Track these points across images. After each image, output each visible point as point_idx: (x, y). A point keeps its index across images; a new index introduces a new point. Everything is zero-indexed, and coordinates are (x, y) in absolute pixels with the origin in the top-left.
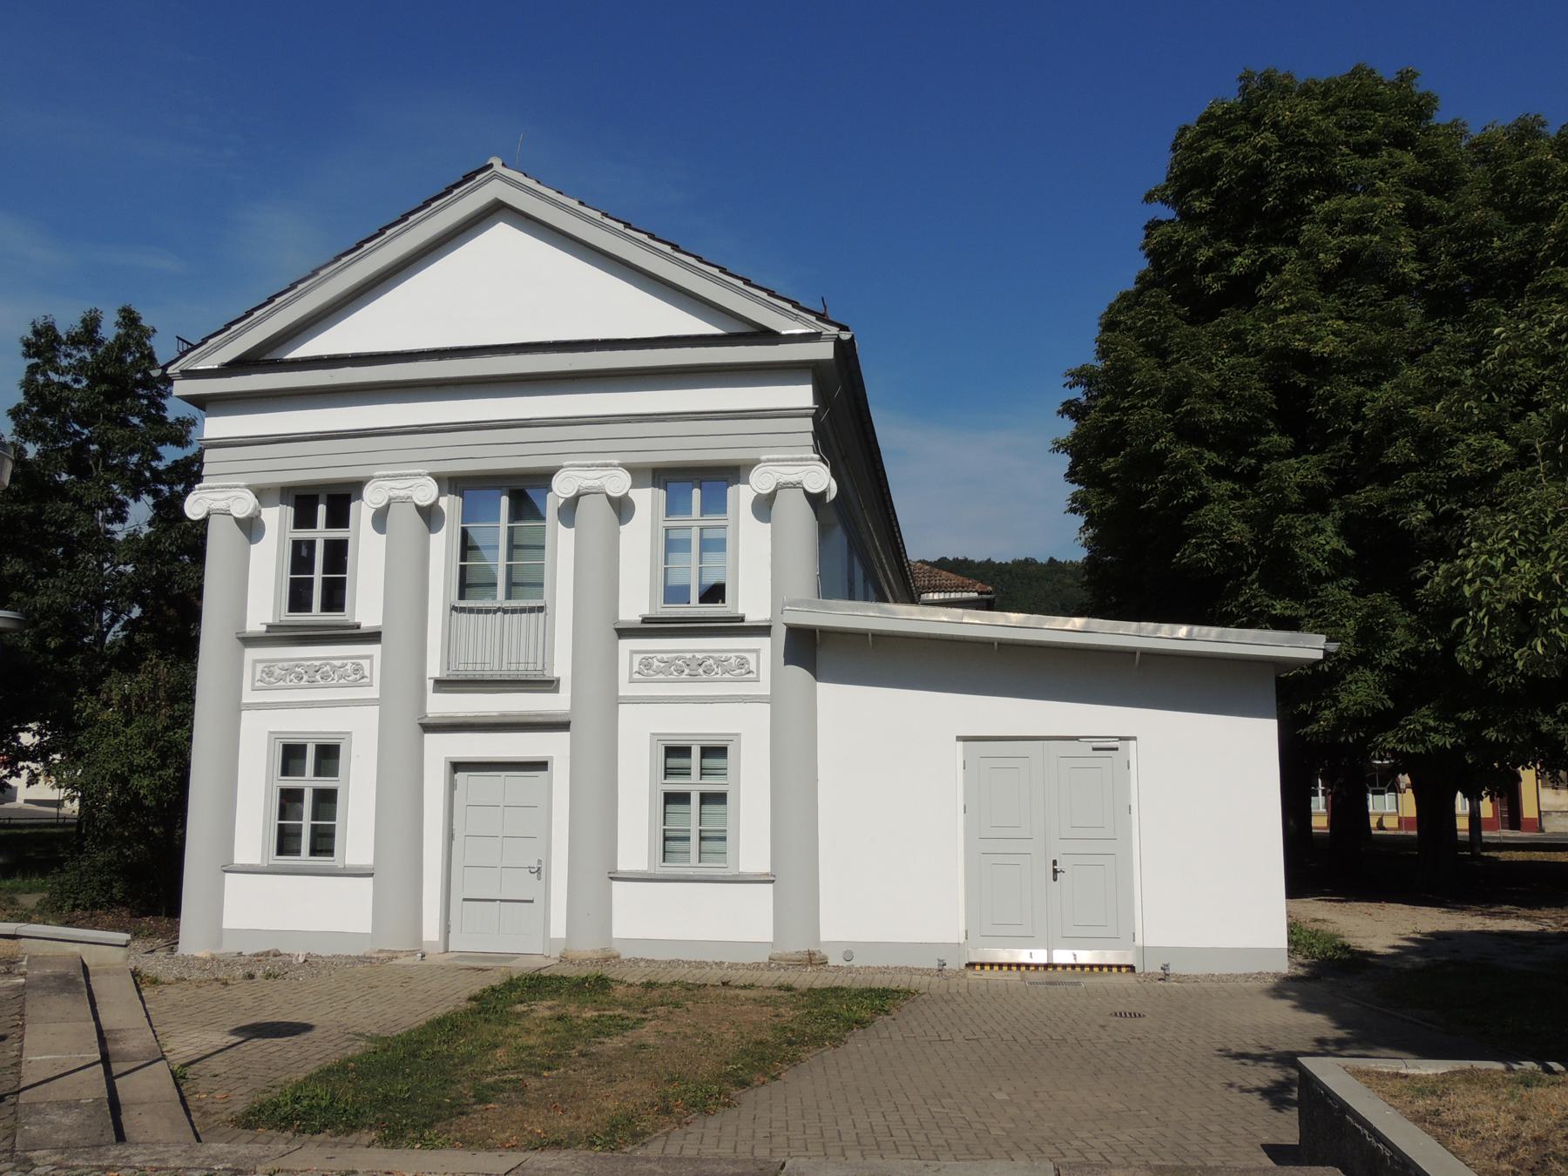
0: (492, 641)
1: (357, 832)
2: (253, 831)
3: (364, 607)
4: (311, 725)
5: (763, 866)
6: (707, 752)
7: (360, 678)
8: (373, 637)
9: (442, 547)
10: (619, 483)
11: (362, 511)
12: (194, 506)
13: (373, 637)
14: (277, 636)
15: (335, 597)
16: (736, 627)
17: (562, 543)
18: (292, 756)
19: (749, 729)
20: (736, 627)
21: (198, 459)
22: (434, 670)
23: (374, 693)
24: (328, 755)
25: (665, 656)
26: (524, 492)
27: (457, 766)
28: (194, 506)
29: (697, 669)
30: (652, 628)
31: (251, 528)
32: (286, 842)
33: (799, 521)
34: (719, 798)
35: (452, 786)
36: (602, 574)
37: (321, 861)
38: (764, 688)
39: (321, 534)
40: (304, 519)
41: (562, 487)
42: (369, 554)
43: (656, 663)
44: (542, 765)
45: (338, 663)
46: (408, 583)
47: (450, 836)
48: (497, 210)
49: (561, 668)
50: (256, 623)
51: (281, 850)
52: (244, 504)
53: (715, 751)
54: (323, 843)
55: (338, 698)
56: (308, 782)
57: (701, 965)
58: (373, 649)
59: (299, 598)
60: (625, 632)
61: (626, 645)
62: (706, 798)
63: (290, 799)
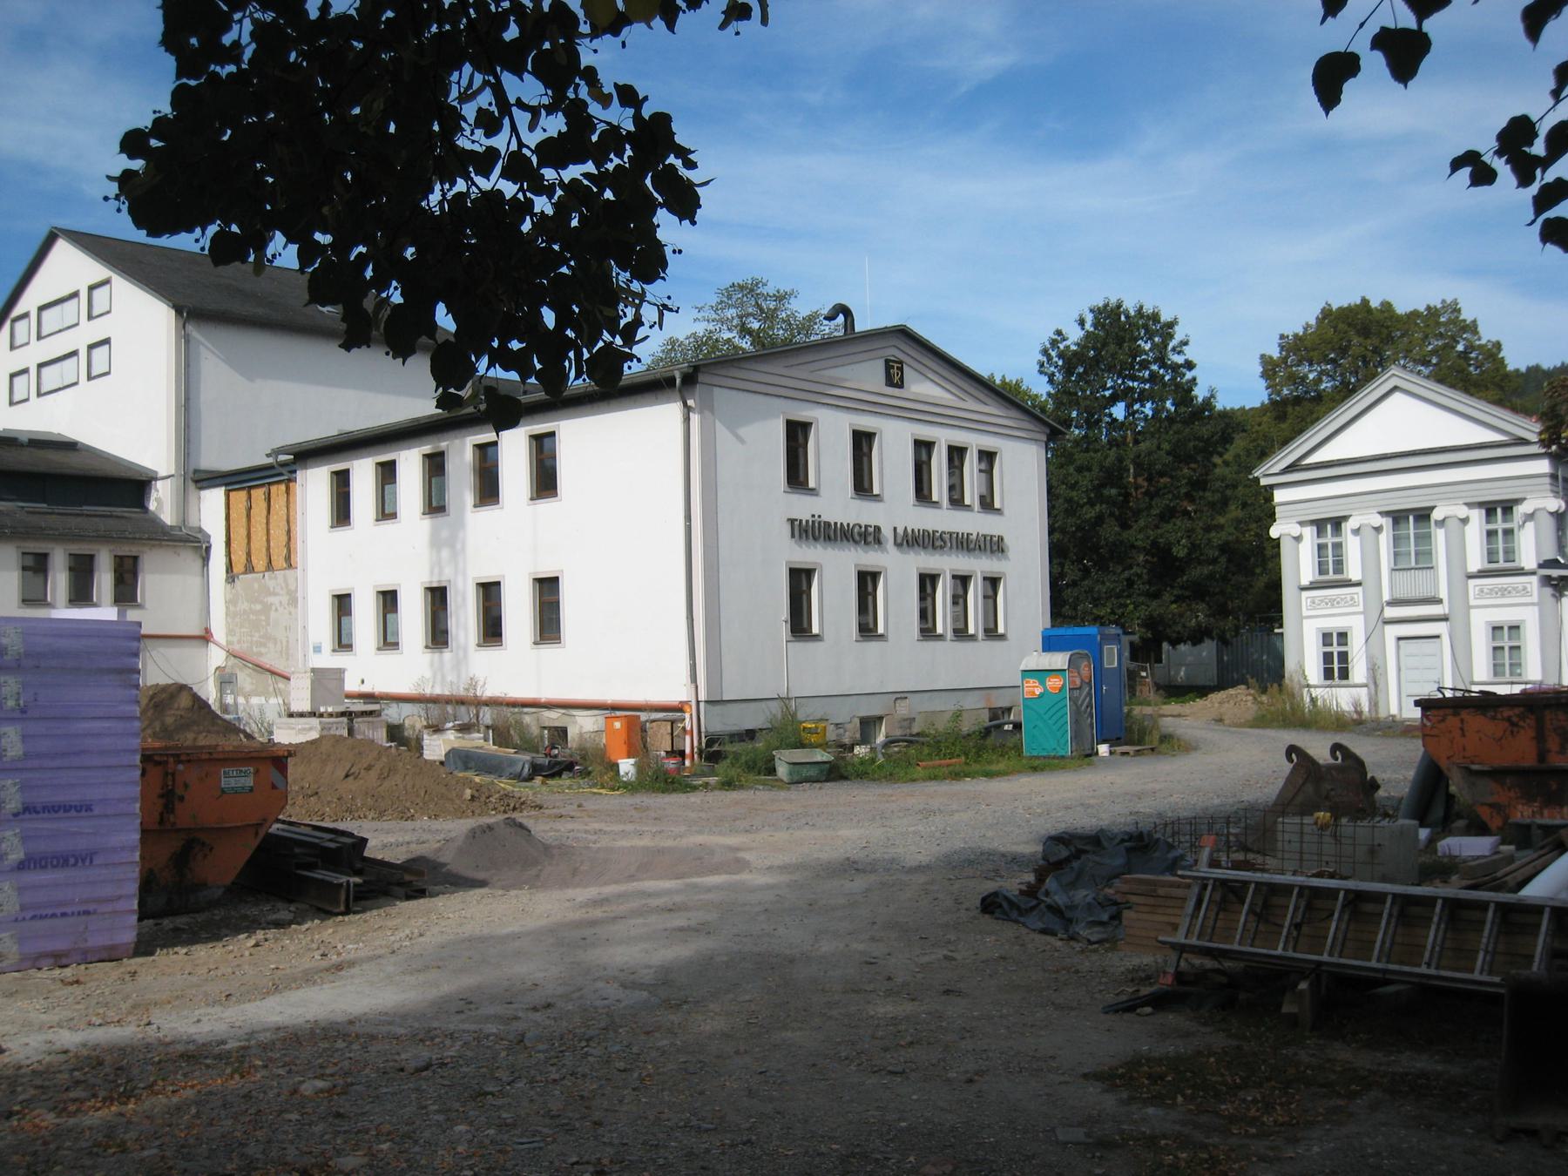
0: (1414, 583)
1: (1359, 672)
2: (1314, 672)
3: (1353, 571)
4: (1505, 616)
5: (1364, 681)
6: (1510, 628)
7: (1525, 591)
8: (1358, 584)
9: (1385, 539)
10: (1463, 512)
11: (1348, 527)
12: (1274, 532)
13: (1358, 584)
14: (1314, 586)
15: (1339, 566)
16: (1520, 572)
17: (1439, 536)
18: (1326, 638)
19: (1529, 618)
20: (1520, 572)
21: (1538, 212)
22: (1386, 597)
23: (1361, 609)
24: (1343, 637)
26: (1423, 515)
27: (1400, 639)
28: (1274, 532)
29: (1504, 592)
30: (1482, 574)
31: (1298, 539)
32: (1328, 674)
33: (1549, 525)
34: (1519, 648)
35: (1398, 648)
36: (1458, 551)
37: (1344, 682)
38: (1535, 599)
39: (1329, 539)
40: (1321, 532)
41: (1437, 515)
42: (1353, 548)
44: (1438, 637)
46: (1370, 559)
47: (1399, 670)
48: (1395, 389)
49: (1443, 594)
50: (1305, 582)
51: (1495, 674)
52: (1295, 530)
53: (1515, 628)
54: (1344, 674)
55: (1346, 613)
56: (1335, 649)
57: (351, 634)
58: (1358, 589)
59: (1322, 570)
60: (1471, 576)
61: (1472, 582)
62: (1511, 648)
63: (1328, 658)
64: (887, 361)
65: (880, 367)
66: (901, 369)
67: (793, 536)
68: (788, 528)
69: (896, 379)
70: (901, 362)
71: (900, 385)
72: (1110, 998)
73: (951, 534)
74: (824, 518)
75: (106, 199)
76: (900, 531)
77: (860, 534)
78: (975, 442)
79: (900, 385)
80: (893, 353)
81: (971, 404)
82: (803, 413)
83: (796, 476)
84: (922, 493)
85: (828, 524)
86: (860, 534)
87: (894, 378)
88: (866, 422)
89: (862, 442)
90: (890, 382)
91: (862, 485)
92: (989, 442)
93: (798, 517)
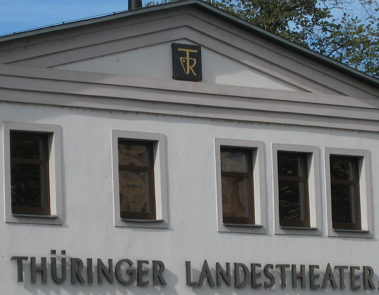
64: (175, 47)
65: (163, 56)
66: (198, 56)
67: (20, 279)
68: (13, 268)
69: (189, 69)
70: (198, 47)
71: (197, 76)
72: (221, 271)
73: (282, 267)
74: (71, 254)
75: (200, 126)
76: (197, 266)
77: (130, 273)
78: (321, 145)
79: (197, 76)
80: (185, 35)
81: (318, 96)
82: (35, 121)
83: (30, 196)
84: (237, 215)
85: (77, 262)
86: (130, 273)
87: (187, 66)
88: (140, 128)
89: (137, 159)
90: (179, 74)
91: (137, 209)
92: (347, 144)
93: (29, 254)
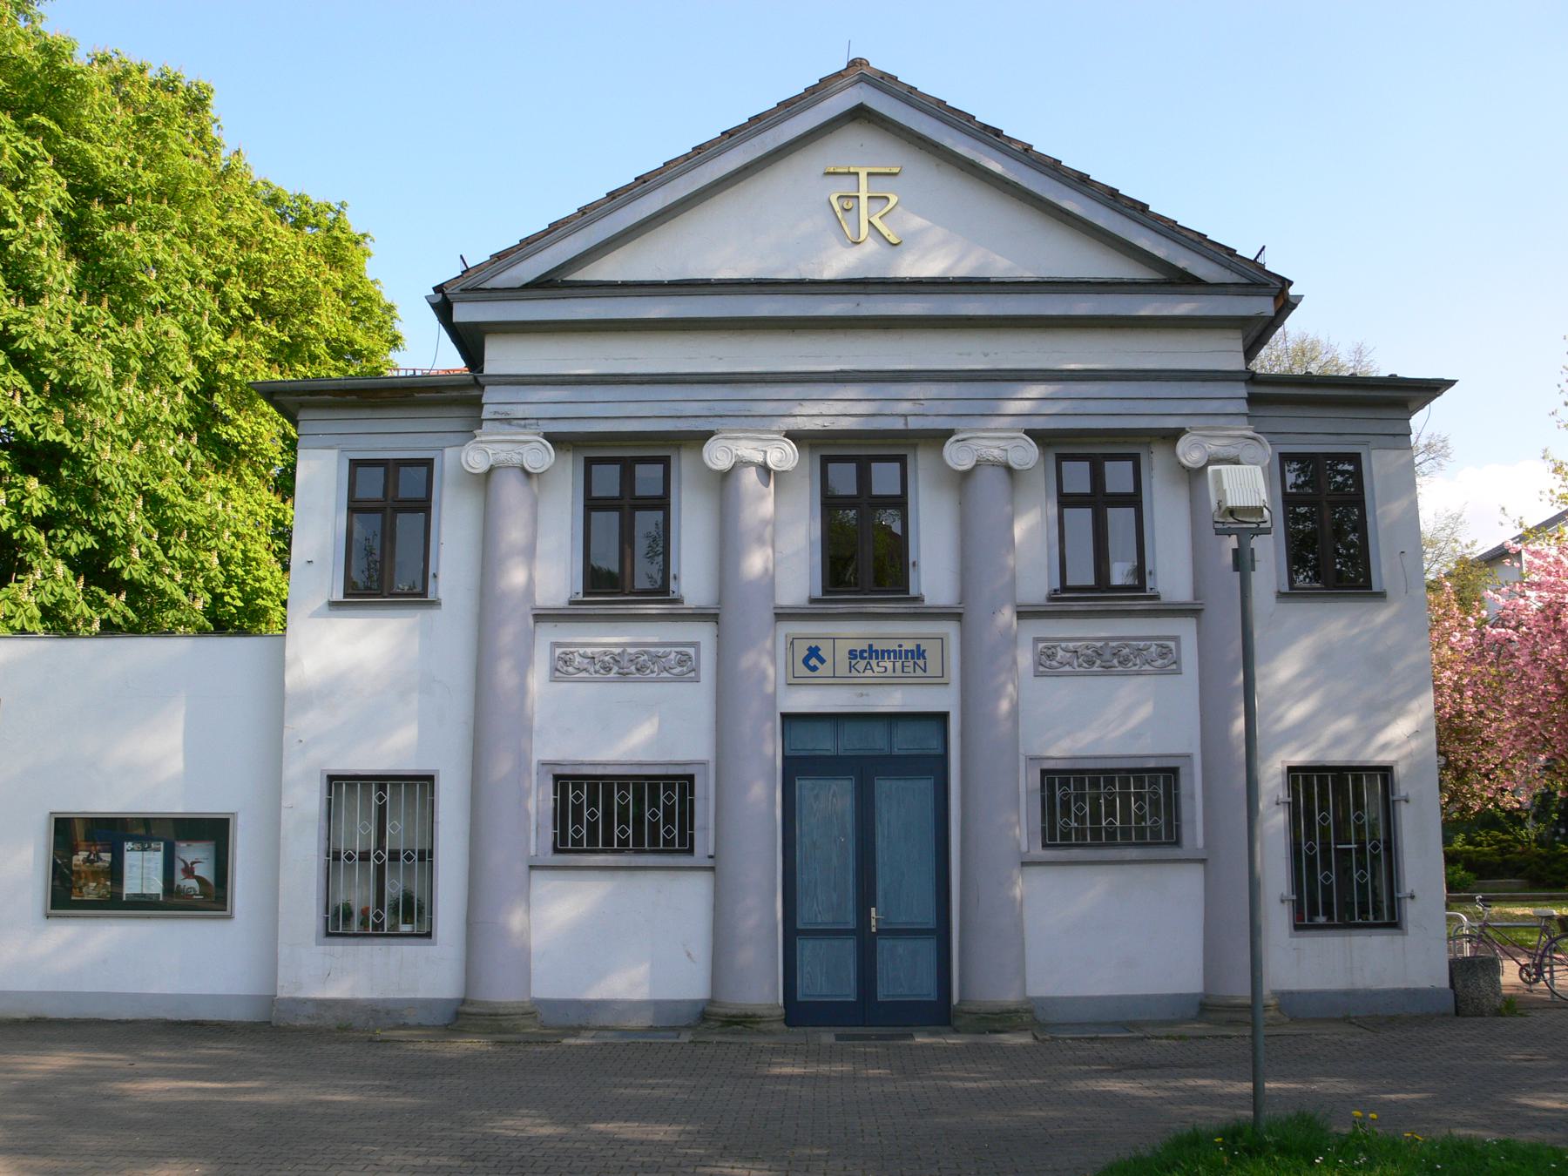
25: (1071, 645)
43: (578, 659)
45: (1142, 644)
